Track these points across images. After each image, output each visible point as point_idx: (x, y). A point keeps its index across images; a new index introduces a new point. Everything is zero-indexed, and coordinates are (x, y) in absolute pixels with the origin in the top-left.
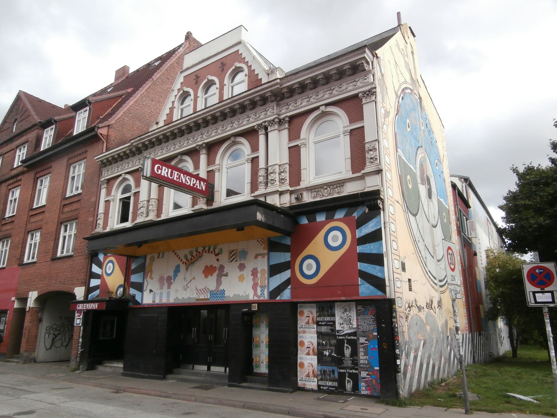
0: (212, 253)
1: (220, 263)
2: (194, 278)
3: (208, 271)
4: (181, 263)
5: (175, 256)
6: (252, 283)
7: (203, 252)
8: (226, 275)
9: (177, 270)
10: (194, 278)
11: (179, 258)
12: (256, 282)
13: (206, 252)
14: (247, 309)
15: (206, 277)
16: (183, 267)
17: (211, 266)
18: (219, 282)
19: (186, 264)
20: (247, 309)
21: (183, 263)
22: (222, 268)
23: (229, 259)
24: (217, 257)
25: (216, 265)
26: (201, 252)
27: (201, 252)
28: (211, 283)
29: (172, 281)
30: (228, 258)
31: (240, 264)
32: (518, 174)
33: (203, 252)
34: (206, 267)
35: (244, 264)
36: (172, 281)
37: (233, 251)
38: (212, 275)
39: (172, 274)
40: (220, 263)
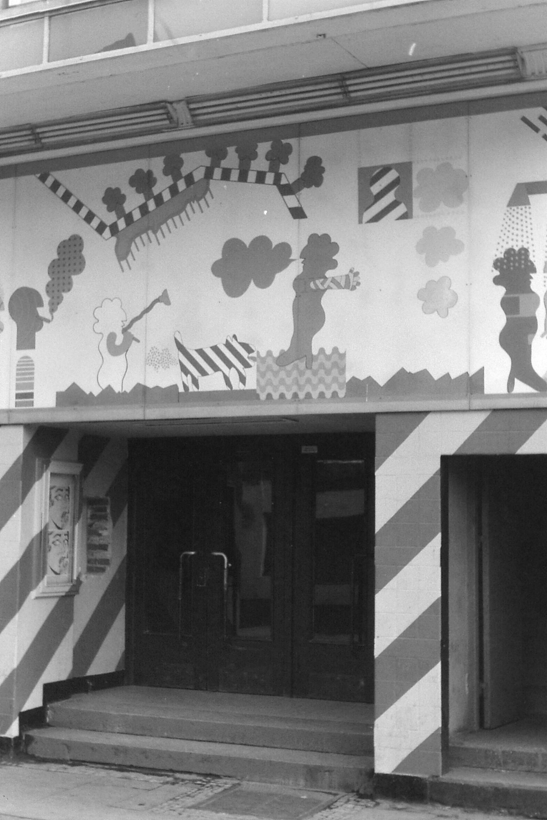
0: (261, 178)
1: (316, 224)
2: (164, 298)
3: (244, 265)
4: (87, 232)
5: (55, 199)
6: (499, 320)
7: (209, 174)
8: (350, 283)
9: (68, 260)
10: (164, 298)
11: (78, 207)
12: (523, 313)
13: (226, 175)
14: (414, 45)
15: (234, 288)
16: (98, 250)
17: (262, 241)
18: (308, 314)
19: (114, 229)
20: (414, 45)
21: (101, 229)
22: (321, 252)
23: (364, 206)
24: (292, 201)
25: (295, 236)
26: (199, 175)
27: (199, 175)
28: (264, 316)
29: (43, 312)
30: (354, 205)
31: (429, 232)
32: (205, 198)
33: (209, 174)
34: (233, 247)
35: (449, 231)
36: (43, 312)
37: (386, 169)
38: (265, 282)
39: (39, 281)
40: (316, 224)
